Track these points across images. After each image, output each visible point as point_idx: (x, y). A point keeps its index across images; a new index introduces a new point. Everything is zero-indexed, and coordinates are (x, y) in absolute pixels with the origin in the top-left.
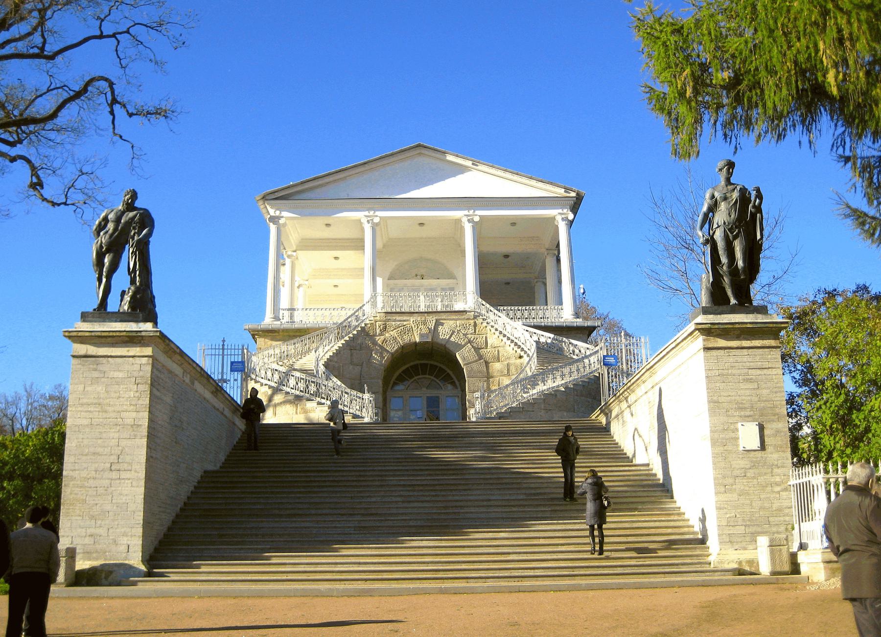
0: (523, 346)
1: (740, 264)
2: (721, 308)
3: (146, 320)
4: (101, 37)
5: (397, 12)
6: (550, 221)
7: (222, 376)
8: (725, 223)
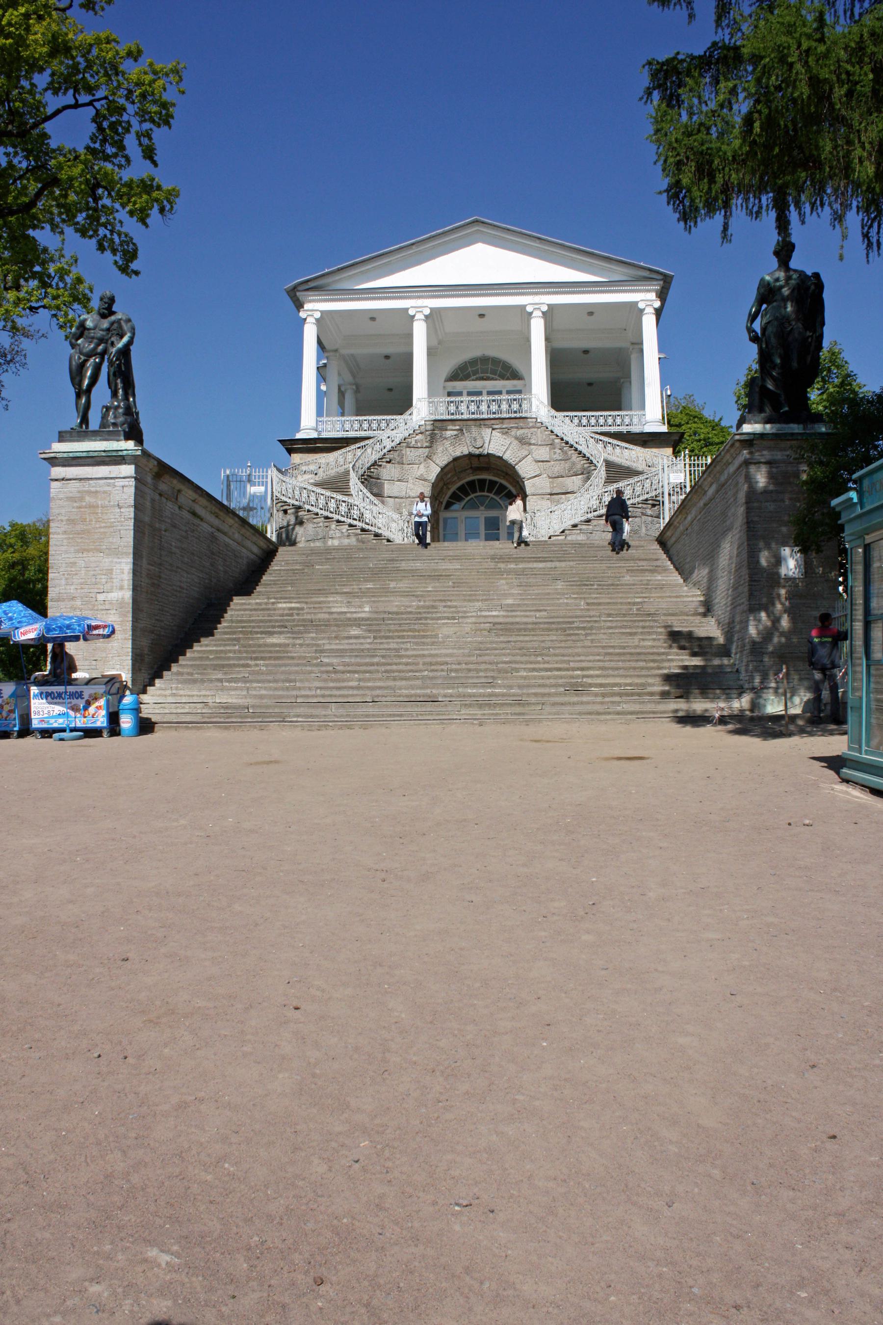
3: (127, 438)
6: (634, 311)
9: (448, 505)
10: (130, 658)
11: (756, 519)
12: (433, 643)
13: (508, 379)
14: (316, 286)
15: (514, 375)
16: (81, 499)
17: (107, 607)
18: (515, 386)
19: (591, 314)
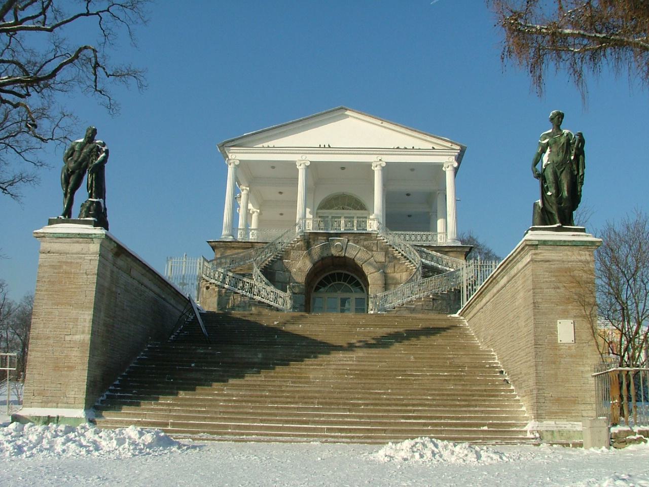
3: (96, 225)
4: (88, 14)
5: (324, 22)
7: (183, 281)
9: (317, 289)
10: (85, 383)
11: (540, 300)
12: (306, 383)
13: (358, 209)
14: (238, 142)
15: (362, 207)
16: (60, 267)
17: (72, 346)
18: (362, 214)
19: (412, 170)
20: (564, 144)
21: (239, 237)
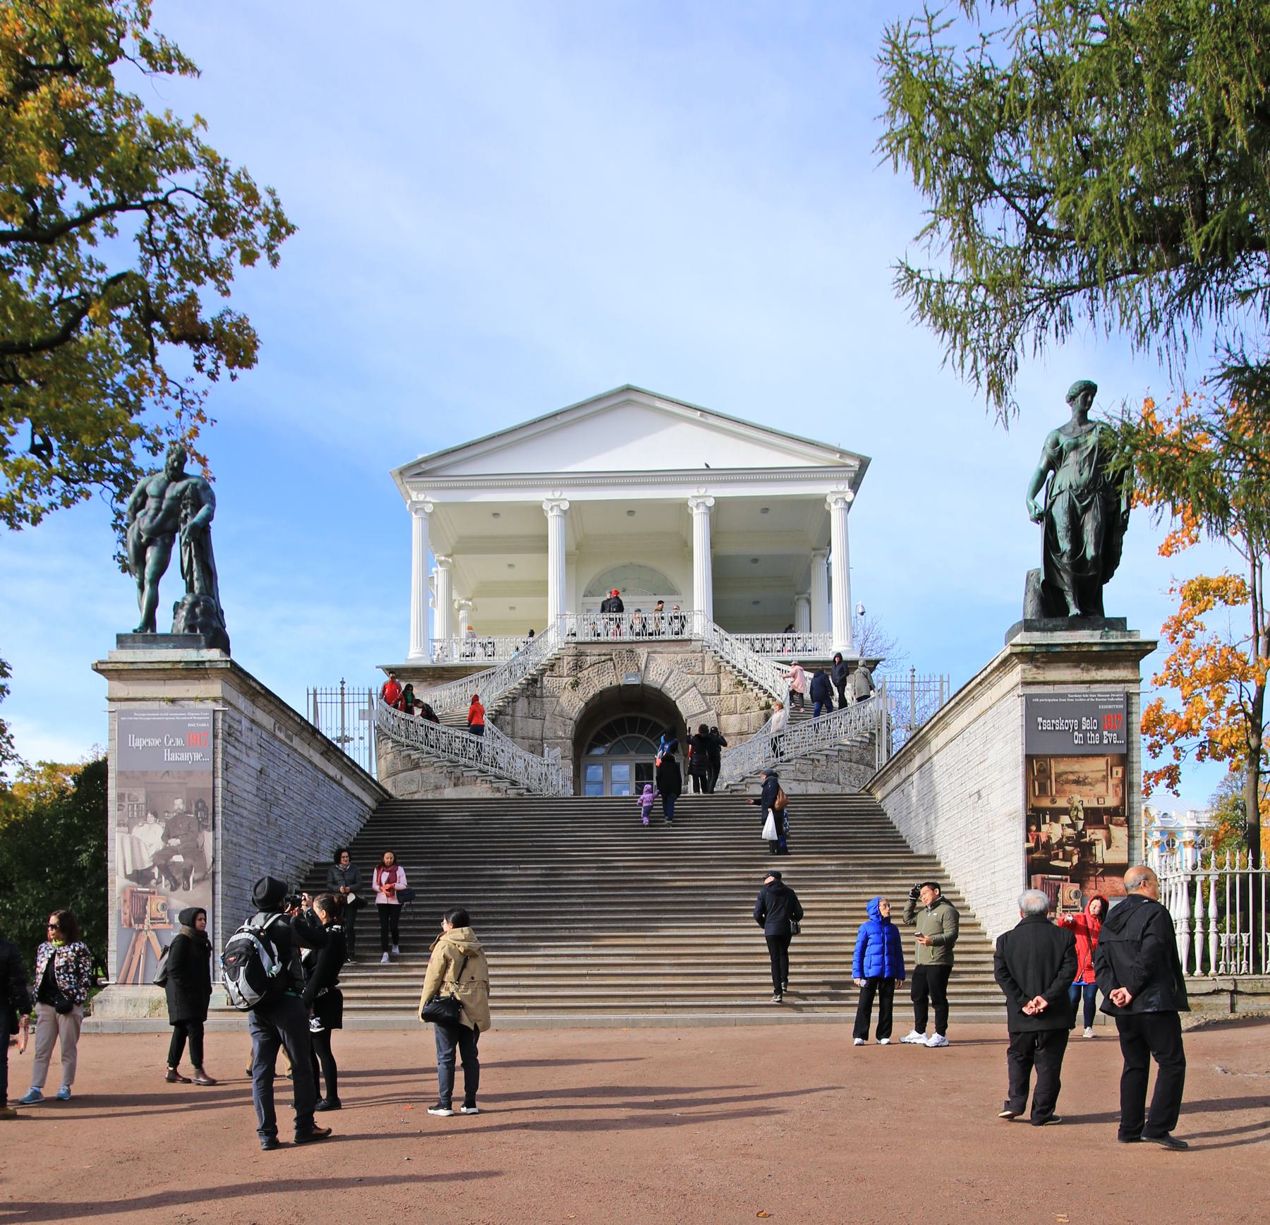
0: (771, 691)
1: (1090, 552)
2: (1052, 623)
3: (211, 645)
8: (1071, 486)
20: (1094, 448)
21: (339, 1080)
